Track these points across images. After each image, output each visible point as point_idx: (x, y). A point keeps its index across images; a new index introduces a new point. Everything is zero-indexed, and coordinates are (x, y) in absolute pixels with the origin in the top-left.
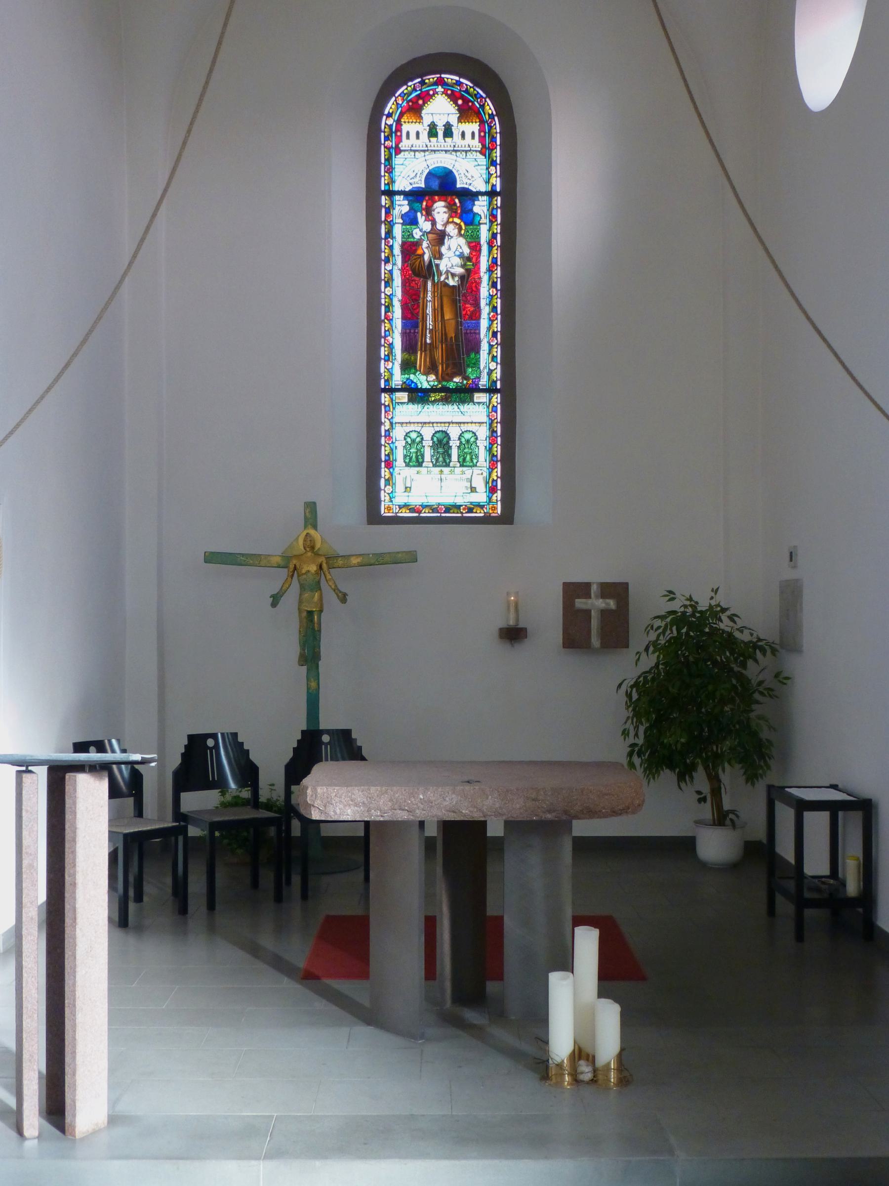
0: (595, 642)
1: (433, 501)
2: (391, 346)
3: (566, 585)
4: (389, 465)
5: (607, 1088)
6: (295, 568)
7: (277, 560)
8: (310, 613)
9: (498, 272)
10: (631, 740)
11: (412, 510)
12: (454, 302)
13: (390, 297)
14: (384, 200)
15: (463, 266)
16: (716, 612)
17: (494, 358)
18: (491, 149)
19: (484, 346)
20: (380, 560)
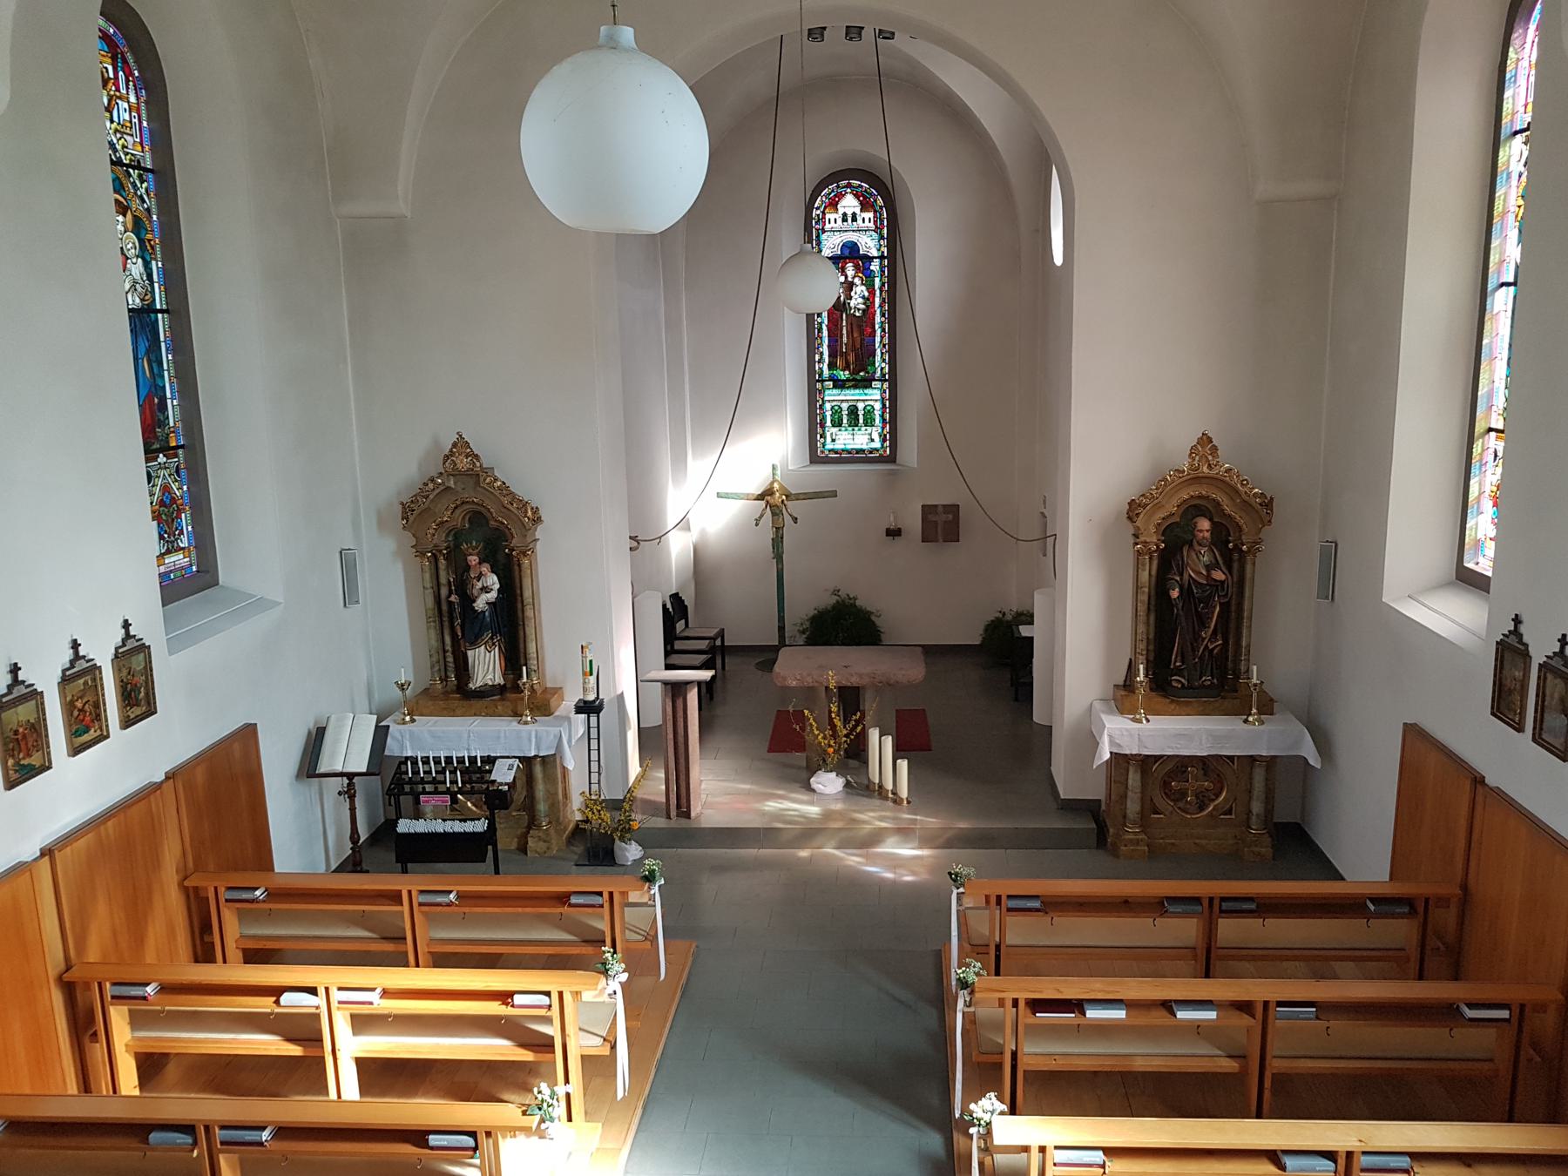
2: (822, 354)
12: (860, 327)
13: (821, 324)
19: (878, 352)
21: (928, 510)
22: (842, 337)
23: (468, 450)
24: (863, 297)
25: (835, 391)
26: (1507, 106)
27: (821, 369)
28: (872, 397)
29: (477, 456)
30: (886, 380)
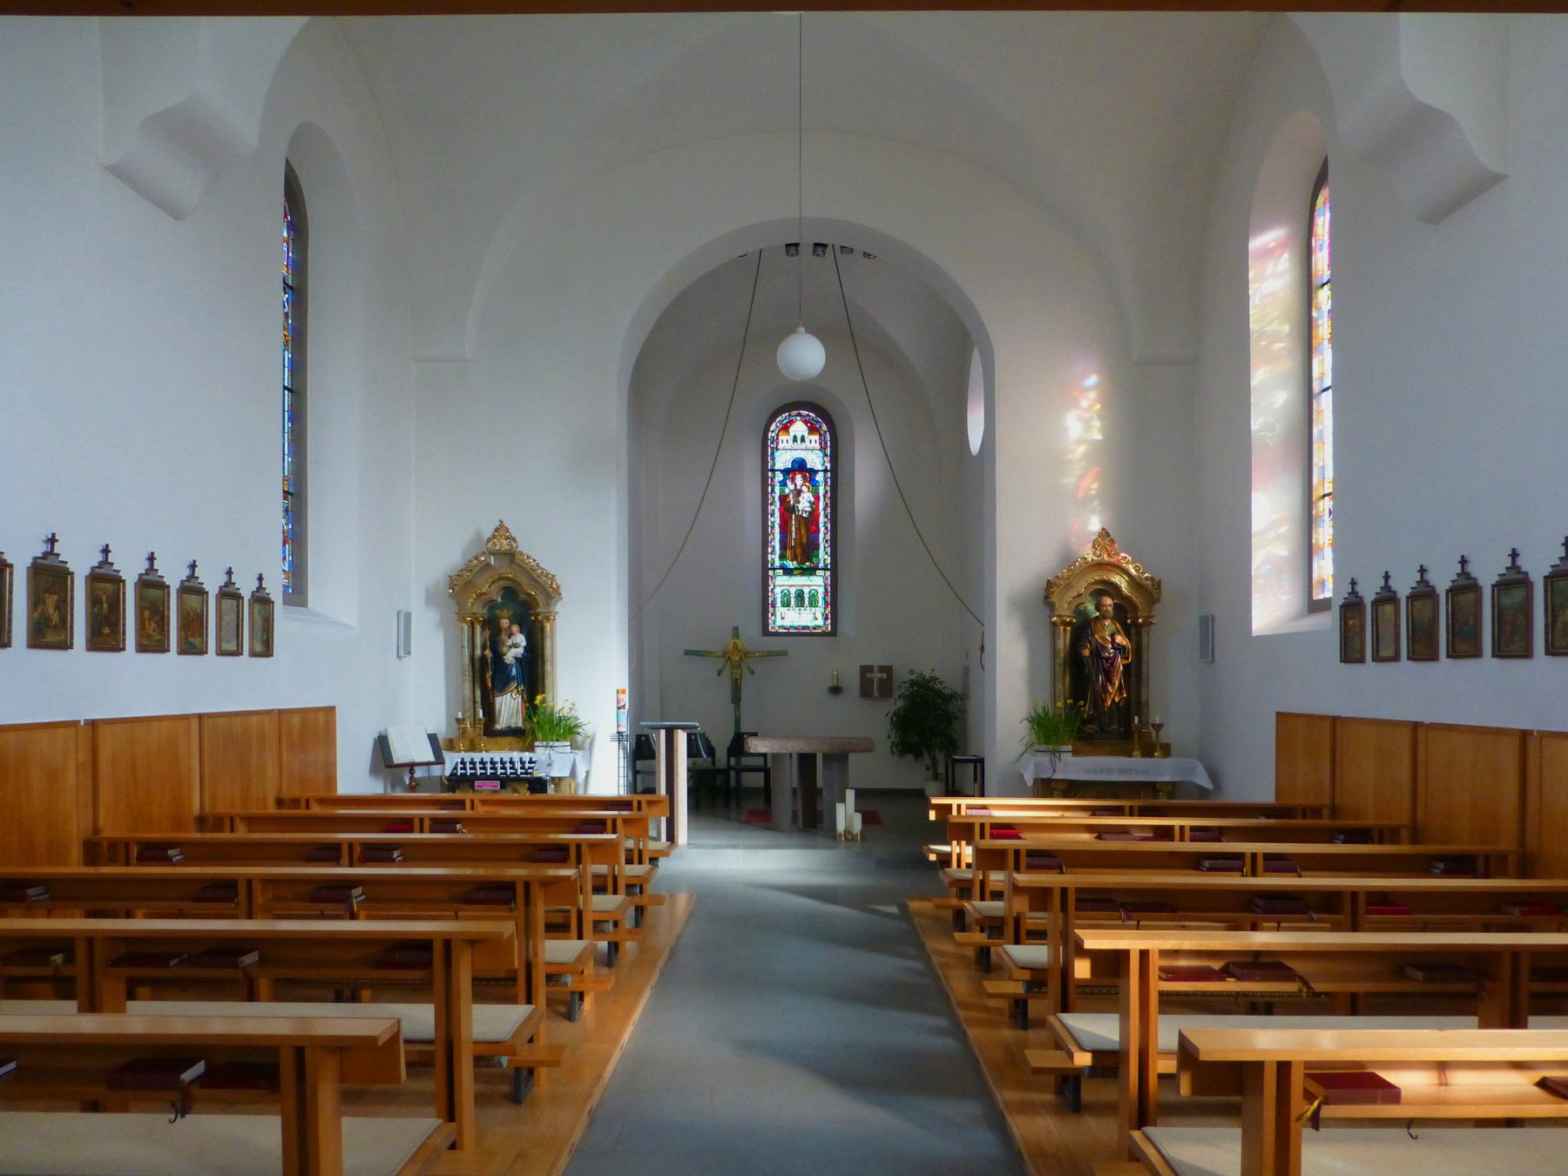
0: (876, 693)
1: (796, 624)
2: (774, 547)
3: (861, 666)
4: (774, 606)
5: (857, 841)
6: (729, 658)
7: (720, 654)
8: (736, 680)
9: (829, 510)
10: (892, 739)
11: (785, 628)
12: (806, 525)
13: (773, 523)
14: (770, 474)
15: (811, 507)
16: (934, 679)
17: (826, 553)
18: (826, 448)
19: (822, 547)
20: (770, 654)
21: (865, 670)
22: (791, 534)
23: (508, 534)
24: (810, 502)
25: (785, 578)
26: (1316, 373)
27: (773, 559)
28: (816, 583)
29: (514, 540)
30: (828, 570)
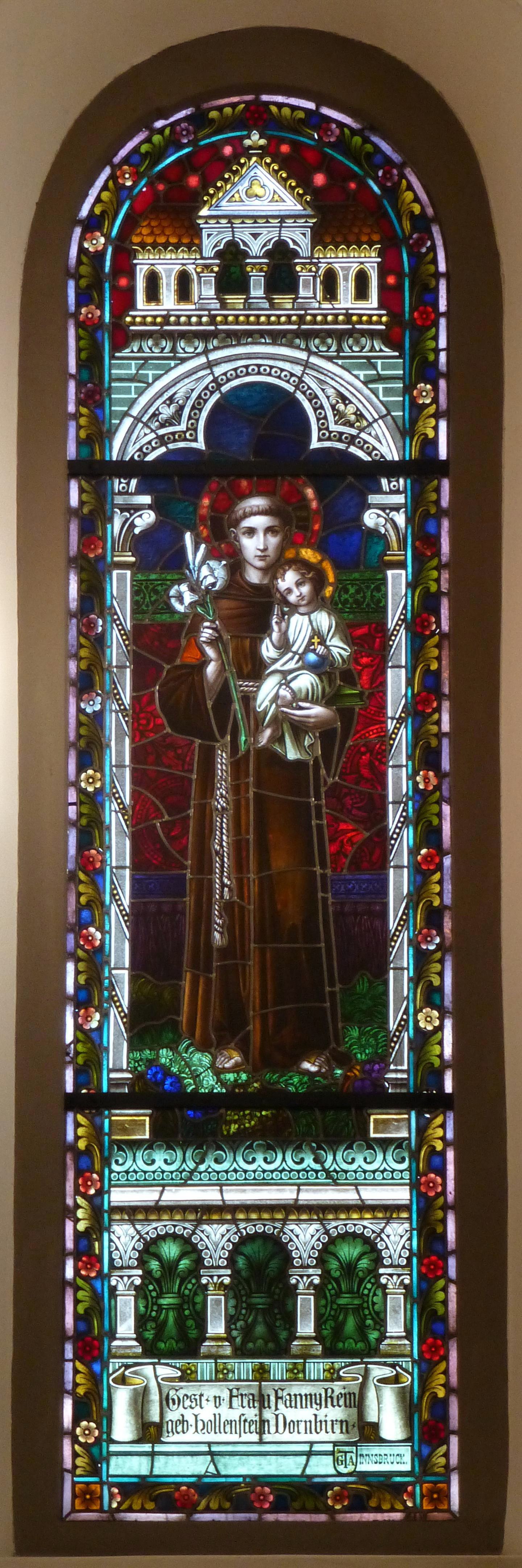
30: (442, 1103)
